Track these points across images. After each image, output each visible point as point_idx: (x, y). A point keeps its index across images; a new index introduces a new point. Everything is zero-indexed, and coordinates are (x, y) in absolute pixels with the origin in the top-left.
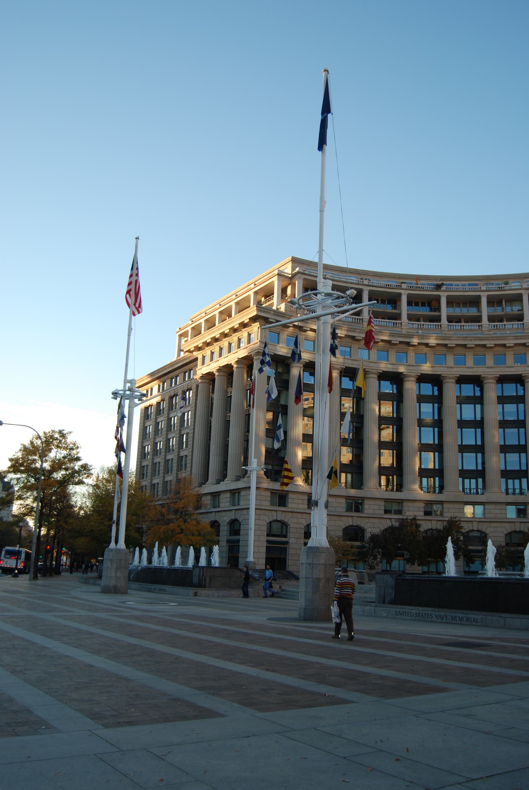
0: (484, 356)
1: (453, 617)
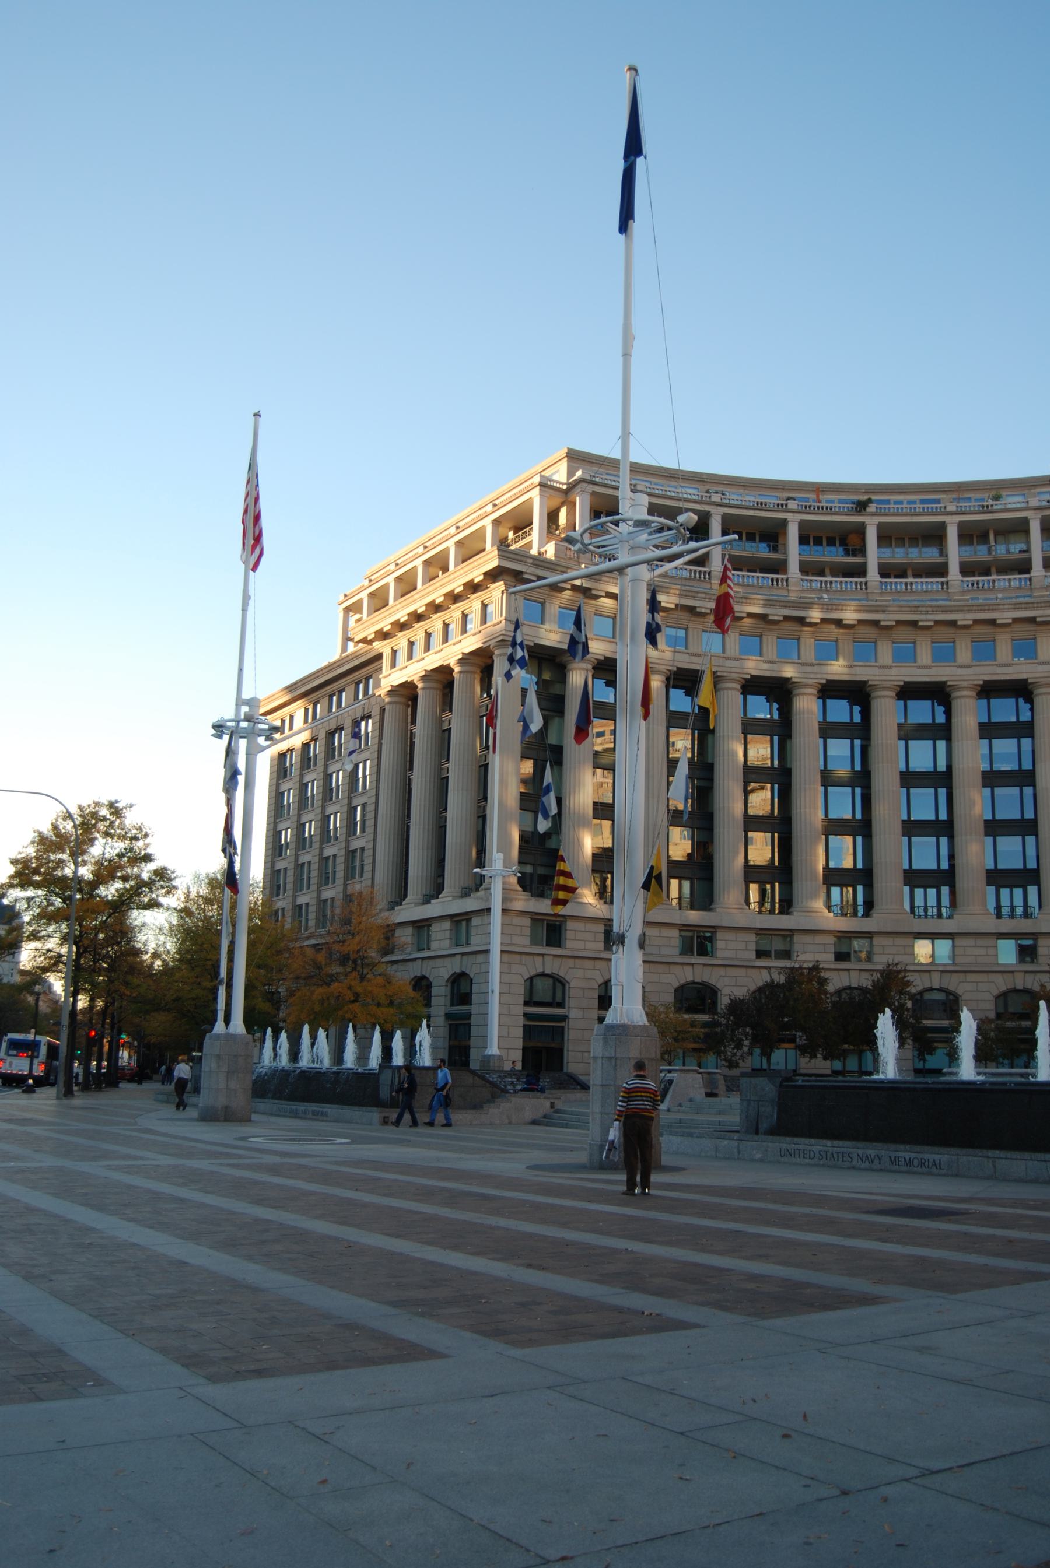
0: (912, 645)
1: (893, 1159)
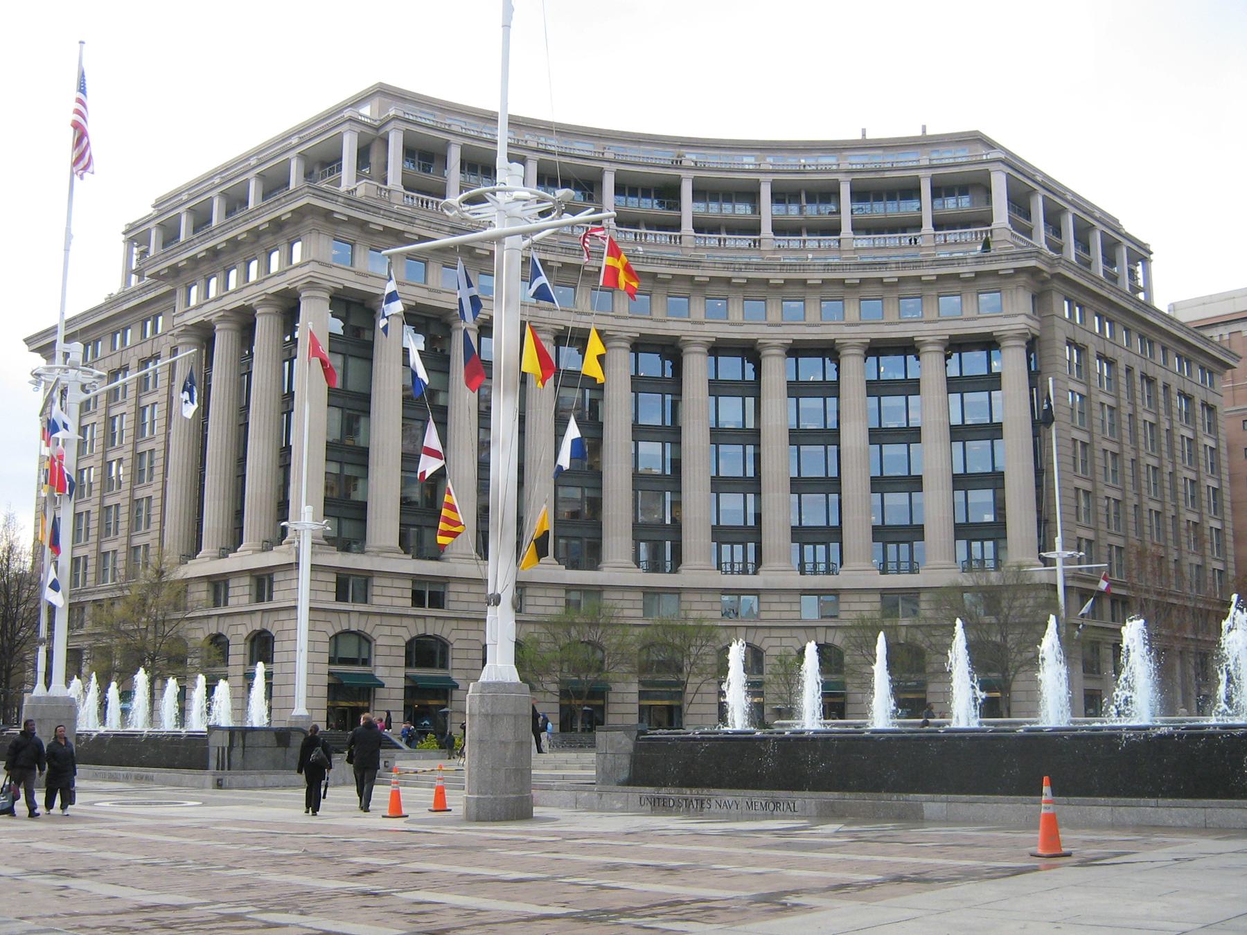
0: (687, 300)
1: (749, 804)
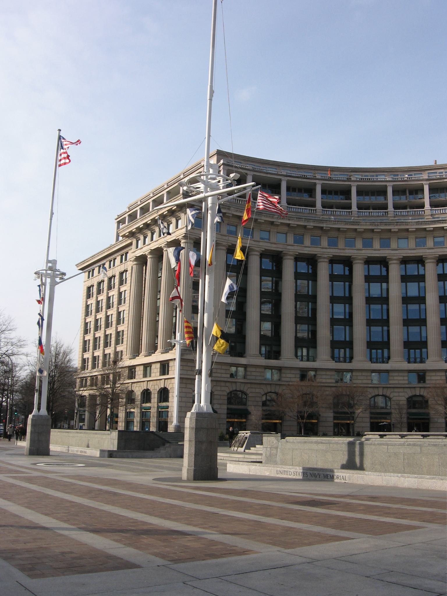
0: (354, 239)
1: (325, 475)
